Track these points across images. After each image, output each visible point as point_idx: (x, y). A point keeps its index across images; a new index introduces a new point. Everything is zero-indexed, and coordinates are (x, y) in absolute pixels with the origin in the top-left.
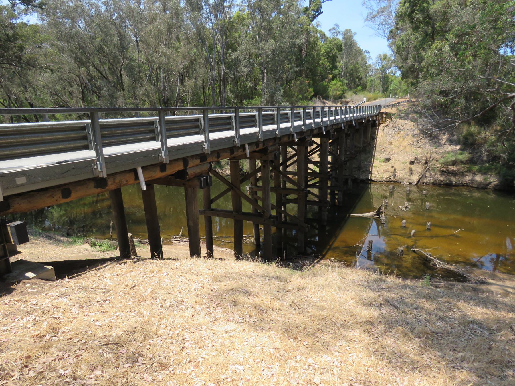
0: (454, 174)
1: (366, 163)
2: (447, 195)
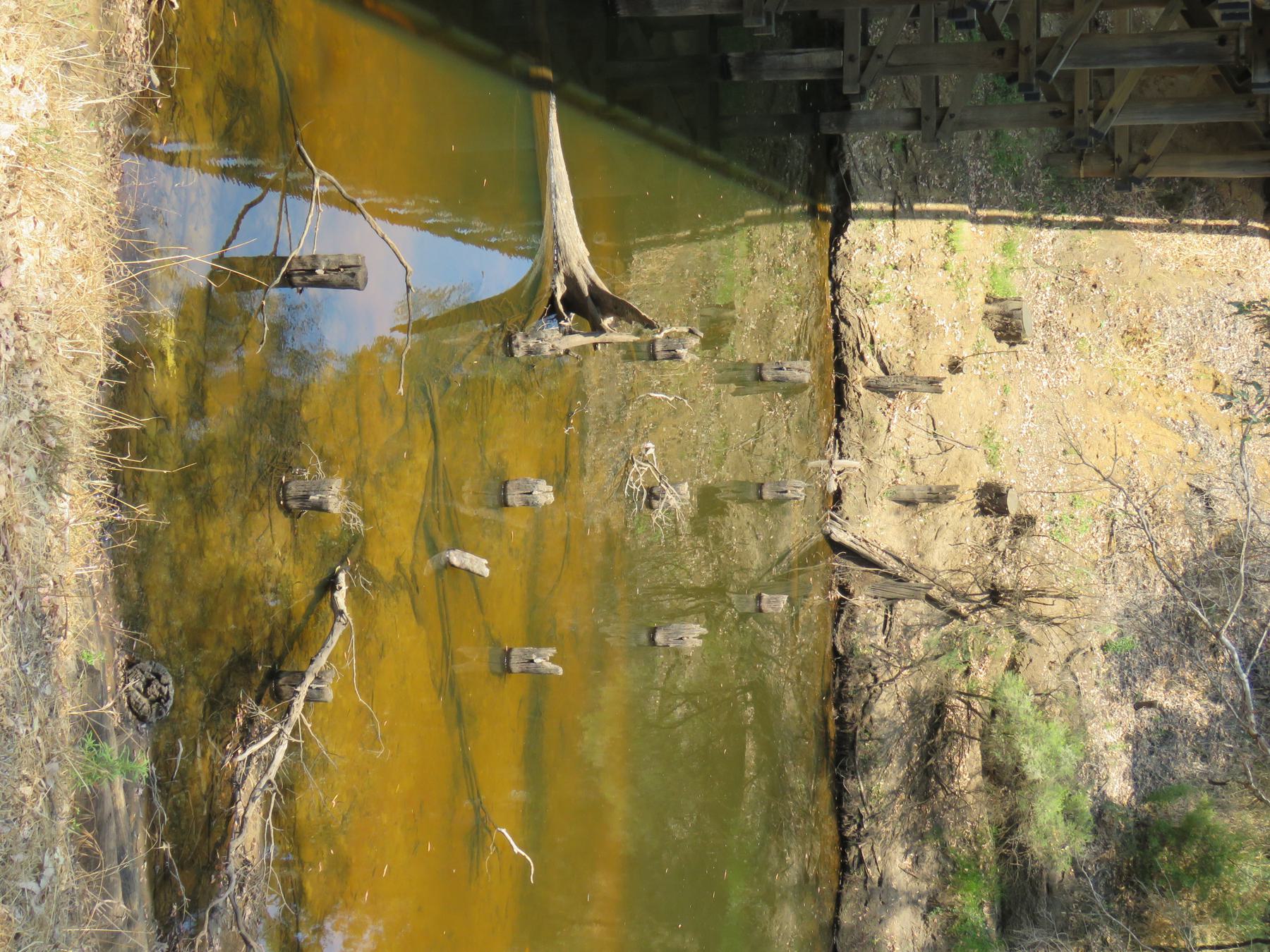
0: (927, 778)
2: (767, 748)
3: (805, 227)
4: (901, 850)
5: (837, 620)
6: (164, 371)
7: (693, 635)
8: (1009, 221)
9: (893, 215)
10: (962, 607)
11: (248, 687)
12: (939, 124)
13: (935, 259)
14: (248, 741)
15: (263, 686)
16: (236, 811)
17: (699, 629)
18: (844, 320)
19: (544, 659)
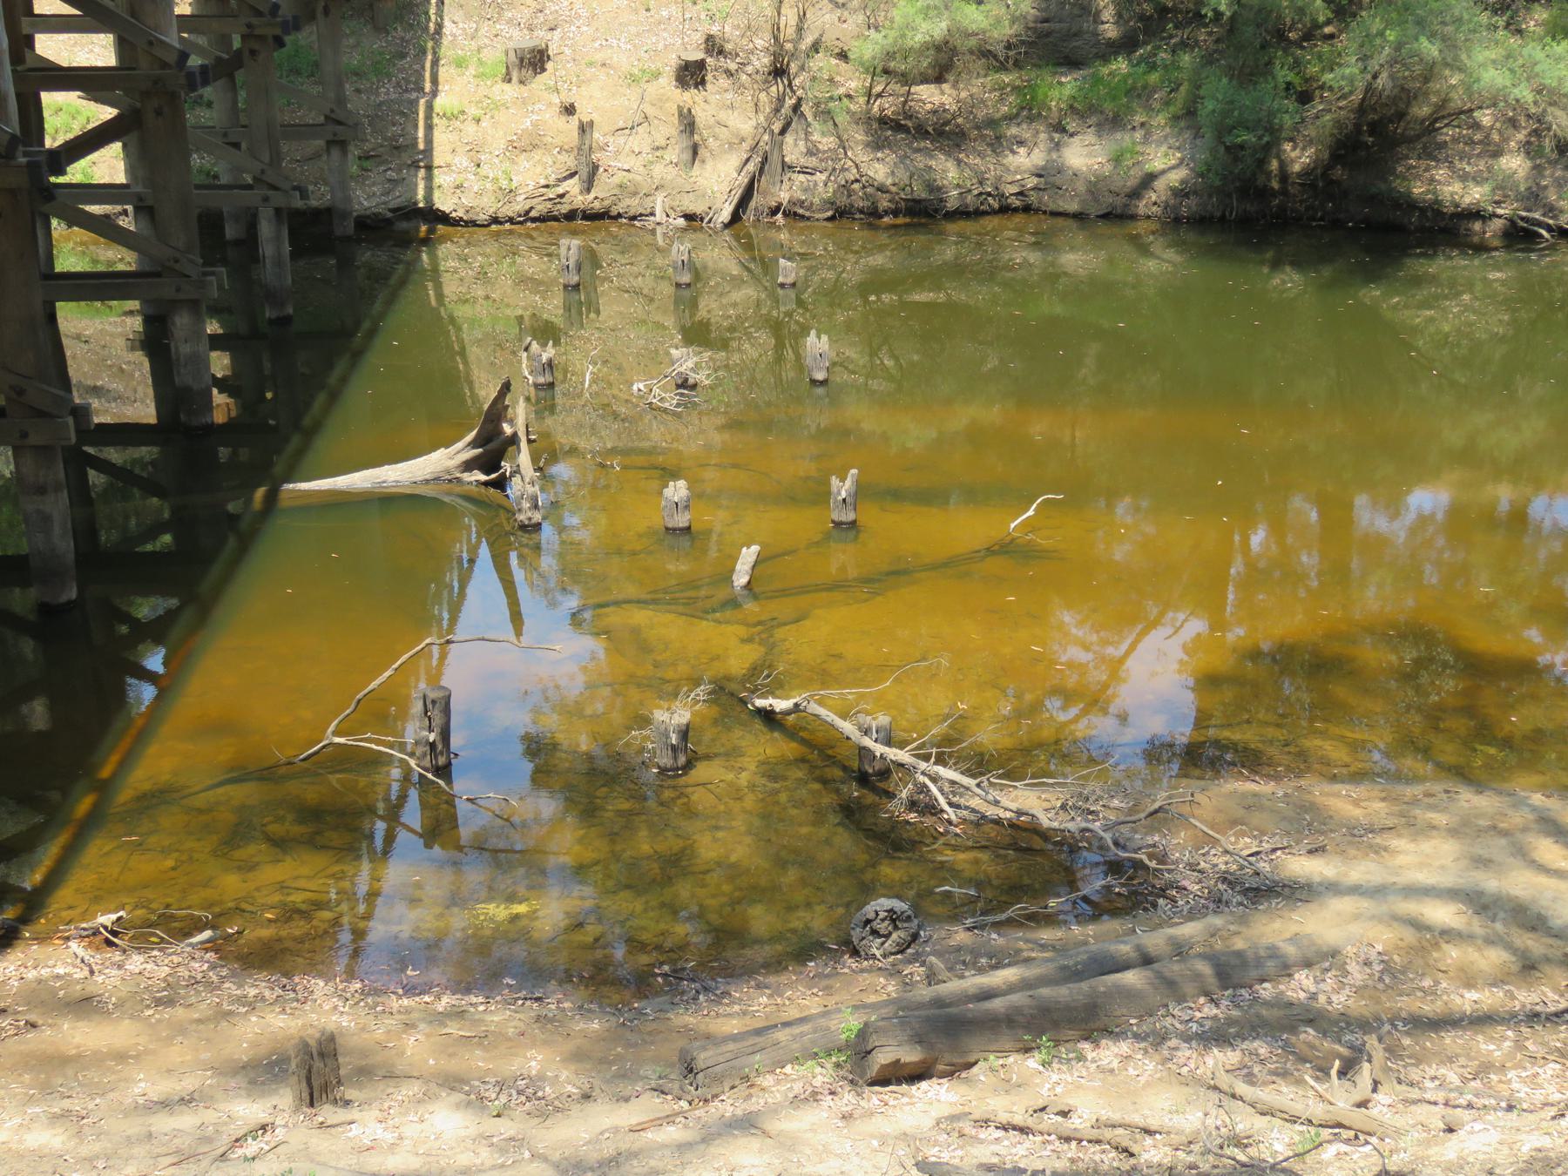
0: (945, 133)
1: (387, 92)
2: (919, 282)
3: (444, 250)
4: (1011, 157)
5: (803, 217)
6: (532, 915)
7: (817, 344)
8: (435, 63)
9: (429, 168)
10: (790, 102)
11: (875, 808)
12: (340, 123)
13: (470, 128)
14: (934, 807)
15: (874, 790)
16: (1009, 820)
17: (812, 338)
18: (527, 212)
19: (843, 488)
